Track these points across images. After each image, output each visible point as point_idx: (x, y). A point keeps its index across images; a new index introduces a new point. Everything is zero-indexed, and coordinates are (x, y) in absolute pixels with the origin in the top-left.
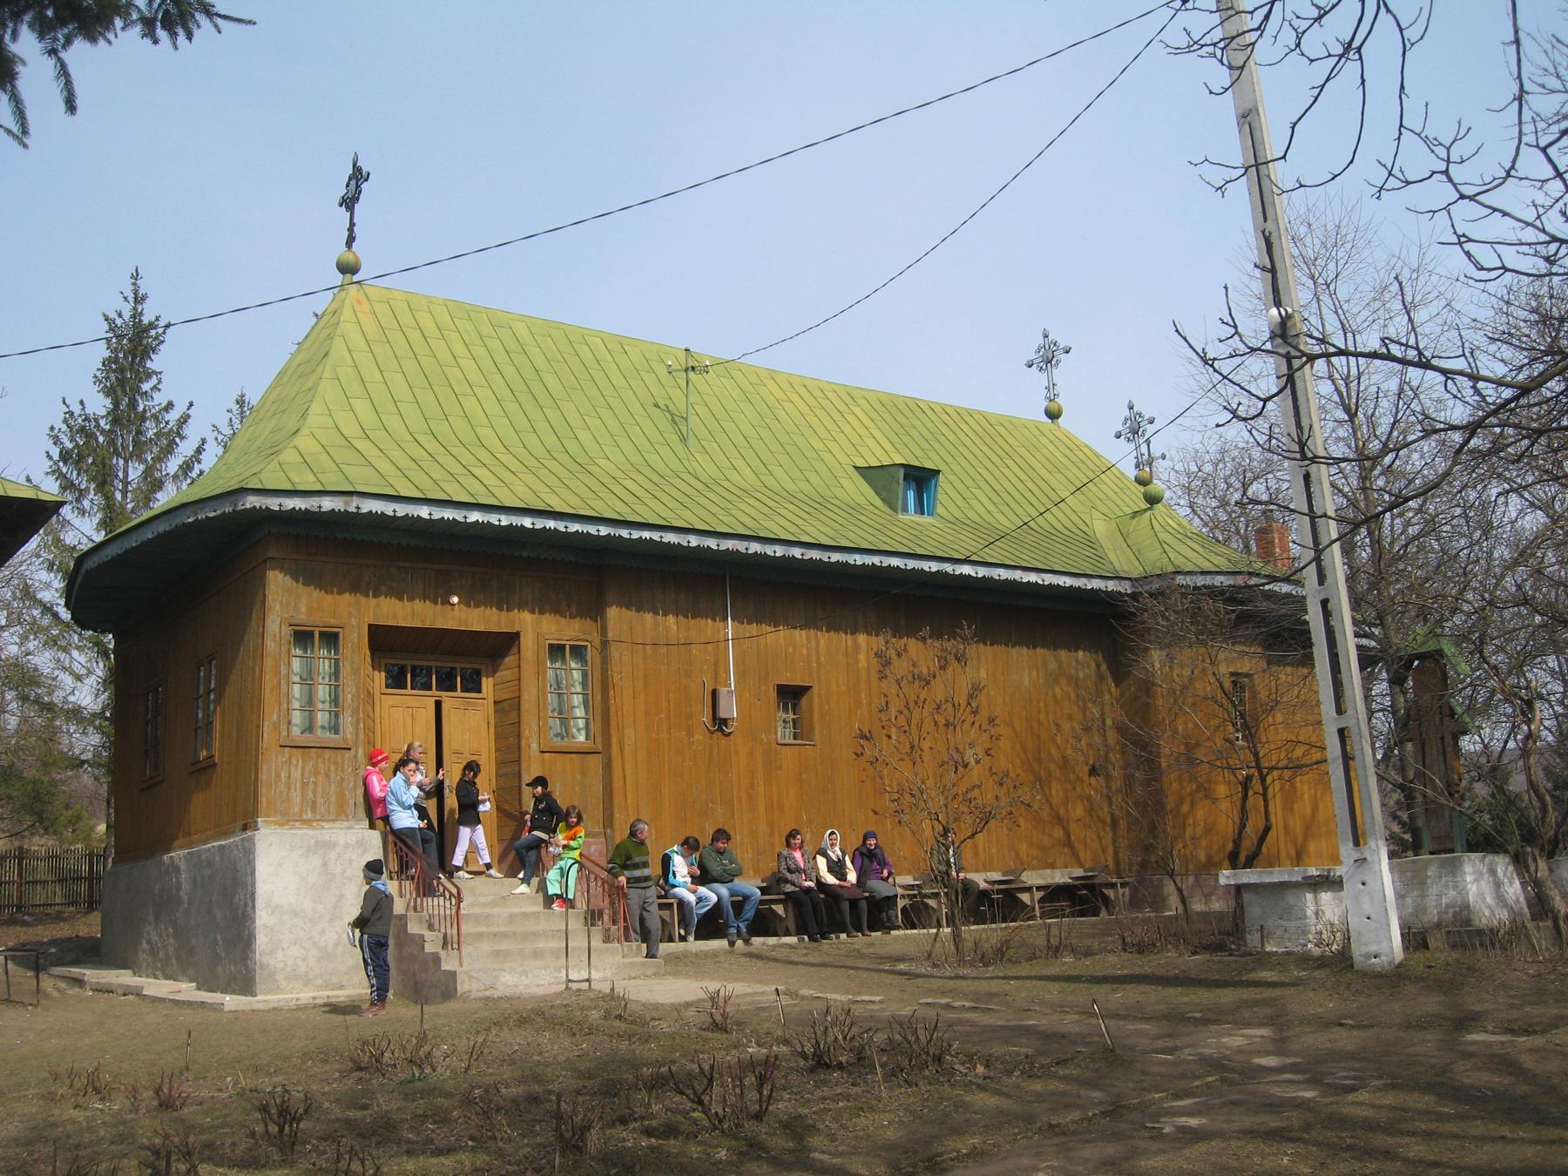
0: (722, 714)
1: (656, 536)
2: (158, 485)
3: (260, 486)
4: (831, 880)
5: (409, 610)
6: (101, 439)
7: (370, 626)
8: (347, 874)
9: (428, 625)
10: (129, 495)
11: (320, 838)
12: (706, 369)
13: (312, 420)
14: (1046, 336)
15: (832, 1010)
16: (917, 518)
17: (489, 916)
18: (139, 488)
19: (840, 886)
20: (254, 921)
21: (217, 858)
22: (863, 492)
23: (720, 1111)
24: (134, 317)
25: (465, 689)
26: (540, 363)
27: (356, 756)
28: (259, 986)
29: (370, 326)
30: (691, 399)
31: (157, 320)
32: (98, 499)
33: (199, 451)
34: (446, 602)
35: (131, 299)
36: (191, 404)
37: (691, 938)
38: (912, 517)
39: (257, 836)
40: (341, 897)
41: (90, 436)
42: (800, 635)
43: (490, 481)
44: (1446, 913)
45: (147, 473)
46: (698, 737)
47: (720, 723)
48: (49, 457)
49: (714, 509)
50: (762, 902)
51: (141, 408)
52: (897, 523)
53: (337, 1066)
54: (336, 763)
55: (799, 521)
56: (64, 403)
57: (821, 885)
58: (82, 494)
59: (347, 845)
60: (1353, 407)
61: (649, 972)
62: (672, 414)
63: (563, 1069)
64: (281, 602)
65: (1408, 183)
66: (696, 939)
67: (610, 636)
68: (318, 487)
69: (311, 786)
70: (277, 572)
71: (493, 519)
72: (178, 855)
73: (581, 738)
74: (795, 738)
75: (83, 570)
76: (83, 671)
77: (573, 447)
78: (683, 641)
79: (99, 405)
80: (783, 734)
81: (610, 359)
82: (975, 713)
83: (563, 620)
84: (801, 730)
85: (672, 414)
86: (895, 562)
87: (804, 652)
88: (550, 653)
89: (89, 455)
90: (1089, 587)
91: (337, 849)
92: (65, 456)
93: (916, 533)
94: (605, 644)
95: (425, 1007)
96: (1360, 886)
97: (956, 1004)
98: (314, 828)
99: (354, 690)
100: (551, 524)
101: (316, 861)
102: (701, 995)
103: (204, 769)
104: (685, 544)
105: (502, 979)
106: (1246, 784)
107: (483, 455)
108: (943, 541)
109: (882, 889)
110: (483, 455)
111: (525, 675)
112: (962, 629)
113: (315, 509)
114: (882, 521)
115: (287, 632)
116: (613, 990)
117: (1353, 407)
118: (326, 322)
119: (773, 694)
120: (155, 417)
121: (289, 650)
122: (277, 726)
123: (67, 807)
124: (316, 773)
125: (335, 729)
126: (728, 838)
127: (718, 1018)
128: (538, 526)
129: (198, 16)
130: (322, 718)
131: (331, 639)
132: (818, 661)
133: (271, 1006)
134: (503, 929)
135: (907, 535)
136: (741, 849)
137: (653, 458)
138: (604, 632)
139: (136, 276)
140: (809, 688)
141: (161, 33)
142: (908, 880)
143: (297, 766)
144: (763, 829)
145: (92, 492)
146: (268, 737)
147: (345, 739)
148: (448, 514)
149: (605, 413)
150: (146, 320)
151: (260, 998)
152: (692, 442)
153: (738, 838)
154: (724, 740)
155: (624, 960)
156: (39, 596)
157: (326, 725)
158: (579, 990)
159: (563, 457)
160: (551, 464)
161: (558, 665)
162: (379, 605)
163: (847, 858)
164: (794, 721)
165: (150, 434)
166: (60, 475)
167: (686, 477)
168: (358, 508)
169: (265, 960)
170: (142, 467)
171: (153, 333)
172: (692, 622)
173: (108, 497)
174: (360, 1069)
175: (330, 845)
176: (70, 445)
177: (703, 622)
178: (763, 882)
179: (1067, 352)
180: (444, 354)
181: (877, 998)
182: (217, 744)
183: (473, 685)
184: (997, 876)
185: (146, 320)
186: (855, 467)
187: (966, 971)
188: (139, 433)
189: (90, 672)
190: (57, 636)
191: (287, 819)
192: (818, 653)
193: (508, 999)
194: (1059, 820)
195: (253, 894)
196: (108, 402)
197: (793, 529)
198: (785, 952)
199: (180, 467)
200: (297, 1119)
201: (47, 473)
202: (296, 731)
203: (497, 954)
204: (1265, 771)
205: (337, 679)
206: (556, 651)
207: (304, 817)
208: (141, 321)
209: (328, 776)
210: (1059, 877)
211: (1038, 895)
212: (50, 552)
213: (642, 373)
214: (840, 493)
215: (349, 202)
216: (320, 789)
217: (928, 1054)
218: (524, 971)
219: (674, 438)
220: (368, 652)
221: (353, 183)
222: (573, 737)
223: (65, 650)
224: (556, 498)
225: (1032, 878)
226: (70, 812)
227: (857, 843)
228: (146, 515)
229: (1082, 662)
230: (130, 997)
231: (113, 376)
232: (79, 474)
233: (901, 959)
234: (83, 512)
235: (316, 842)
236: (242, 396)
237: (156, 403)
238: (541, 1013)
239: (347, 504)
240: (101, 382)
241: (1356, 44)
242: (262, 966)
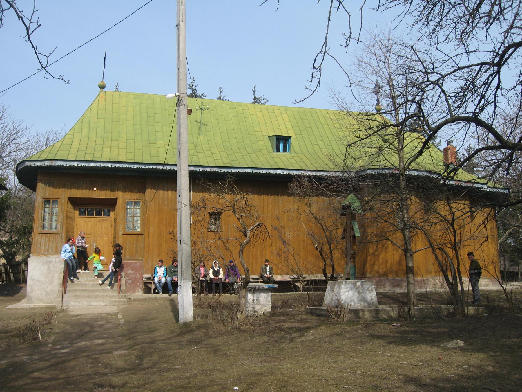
1: (154, 167)
5: (81, 193)
8: (55, 271)
9: (87, 197)
17: (86, 284)
27: (62, 236)
34: (93, 190)
37: (161, 293)
40: (53, 277)
61: (122, 304)
66: (162, 294)
69: (47, 245)
70: (40, 183)
71: (98, 165)
73: (139, 230)
83: (132, 194)
86: (248, 171)
91: (53, 263)
98: (47, 257)
100: (118, 165)
101: (46, 266)
105: (71, 304)
113: (43, 165)
148: (83, 164)
155: (119, 300)
168: (55, 164)
175: (50, 262)
191: (39, 254)
203: (76, 296)
207: (45, 254)
209: (53, 242)
218: (79, 301)
222: (136, 229)
239: (52, 163)
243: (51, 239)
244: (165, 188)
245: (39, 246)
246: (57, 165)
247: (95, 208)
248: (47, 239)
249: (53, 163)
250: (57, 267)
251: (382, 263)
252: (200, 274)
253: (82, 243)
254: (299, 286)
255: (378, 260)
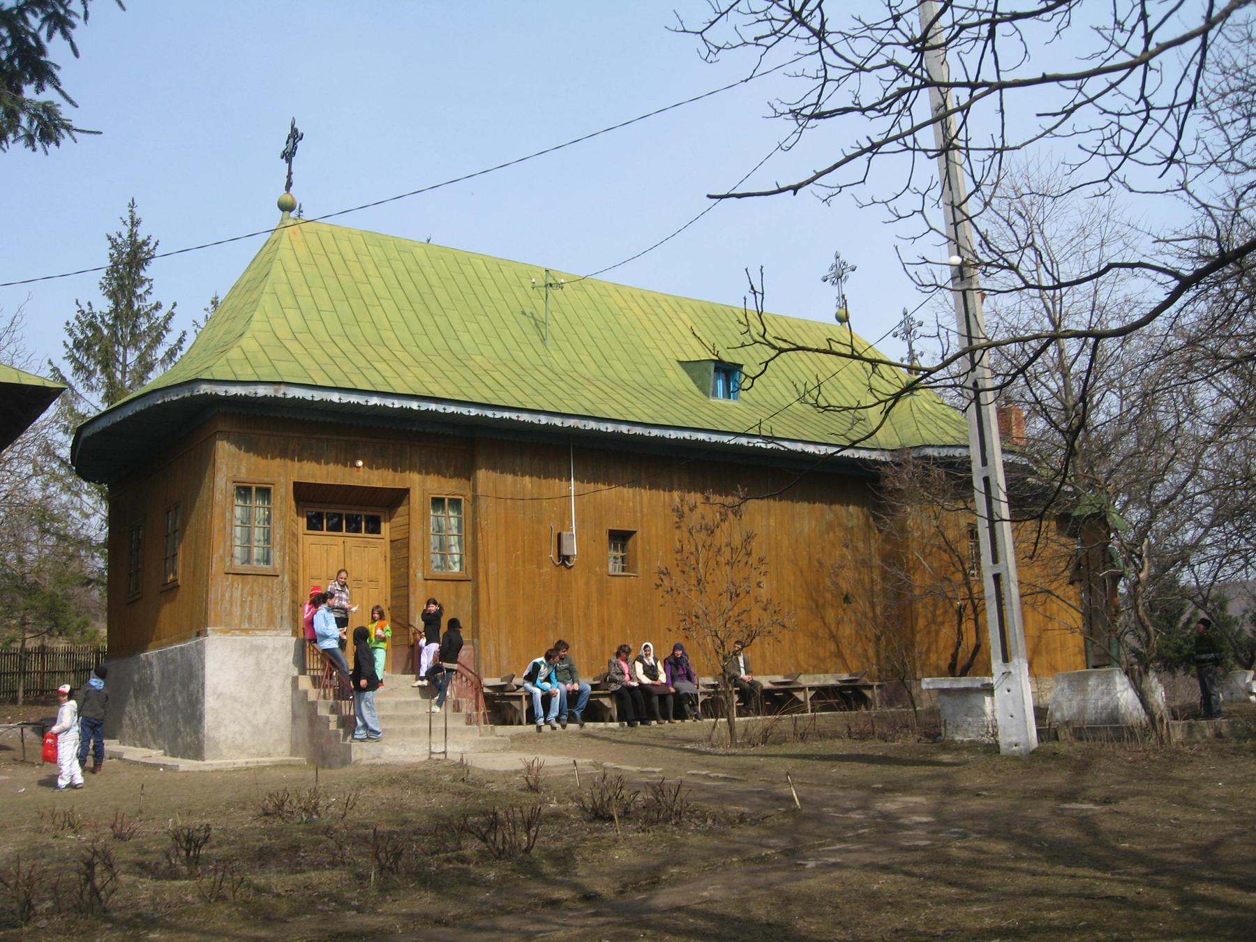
0: (565, 552)
1: (514, 416)
2: (150, 367)
3: (211, 378)
4: (646, 680)
6: (106, 332)
7: (295, 483)
10: (127, 375)
11: (254, 643)
12: (561, 286)
13: (255, 325)
14: (837, 258)
15: (608, 776)
16: (322, 510)
18: (134, 370)
19: (653, 685)
20: (203, 705)
21: (179, 657)
22: (683, 381)
23: (501, 847)
24: (130, 236)
25: (368, 531)
26: (434, 280)
27: (282, 582)
28: (207, 753)
29: (302, 252)
30: (550, 306)
31: (149, 238)
32: (104, 378)
33: (181, 341)
34: (354, 465)
35: (129, 223)
36: (175, 305)
38: (720, 401)
39: (206, 642)
40: (270, 687)
41: (96, 329)
42: (628, 492)
43: (388, 373)
44: (1101, 713)
45: (141, 358)
46: (546, 569)
47: (564, 559)
48: (66, 345)
49: (561, 394)
50: (592, 696)
51: (136, 308)
52: (708, 406)
53: (251, 812)
54: (267, 586)
55: (628, 404)
56: (77, 303)
57: (641, 684)
58: (90, 374)
59: (275, 649)
60: (1057, 321)
61: (499, 748)
62: (535, 320)
63: (658, 845)
64: (227, 465)
65: (900, 218)
67: (479, 491)
68: (255, 378)
69: (248, 604)
70: (225, 442)
71: (389, 402)
72: (151, 654)
73: (456, 569)
74: (623, 571)
75: (82, 438)
76: (91, 511)
77: (455, 346)
78: (535, 496)
79: (103, 305)
80: (613, 567)
81: (489, 276)
82: (749, 554)
84: (627, 564)
85: (535, 320)
86: (702, 436)
87: (631, 504)
88: (433, 503)
89: (96, 344)
90: (856, 456)
92: (78, 345)
93: (720, 413)
94: (475, 498)
95: (319, 769)
96: (1006, 692)
97: (712, 775)
99: (282, 532)
100: (433, 407)
101: (251, 660)
102: (521, 766)
103: (171, 589)
104: (537, 422)
105: (387, 751)
106: (960, 612)
107: (384, 352)
108: (742, 420)
109: (685, 687)
110: (384, 352)
111: (413, 521)
112: (737, 491)
114: (694, 404)
115: (231, 487)
116: (462, 759)
117: (1057, 321)
118: (268, 254)
119: (606, 537)
120: (147, 314)
121: (233, 501)
122: (222, 558)
123: (78, 615)
124: (252, 594)
125: (267, 561)
126: (567, 647)
127: (532, 782)
128: (423, 408)
129: (63, 131)
130: (257, 552)
131: (265, 493)
132: (641, 512)
133: (214, 768)
134: (390, 713)
135: (713, 415)
136: (577, 655)
137: (518, 355)
138: (475, 489)
139: (132, 205)
140: (635, 532)
141: (38, 144)
142: (710, 680)
143: (237, 588)
144: (596, 640)
145: (98, 372)
146: (216, 566)
147: (274, 569)
148: (354, 399)
149: (482, 319)
150: (140, 239)
151: (207, 762)
152: (549, 341)
153: (576, 647)
154: (566, 572)
155: (481, 738)
156: (57, 453)
157: (260, 558)
158: (438, 760)
159: (447, 355)
160: (436, 359)
161: (439, 513)
162: (301, 467)
163: (659, 664)
164: (623, 558)
165: (144, 327)
166: (75, 360)
167: (543, 369)
168: (285, 394)
169: (211, 734)
170: (137, 353)
171: (145, 249)
172: (543, 481)
173: (111, 377)
174: (267, 814)
176: (81, 337)
177: (551, 481)
178: (594, 680)
179: (854, 270)
180: (358, 274)
181: (657, 770)
182: (180, 571)
183: (374, 527)
184: (780, 679)
185: (140, 239)
186: (679, 362)
187: (734, 750)
188: (135, 326)
189: (96, 511)
190: (71, 483)
191: (229, 629)
192: (642, 507)
193: (388, 765)
194: (833, 637)
195: (203, 684)
196: (111, 303)
197: (623, 411)
198: (606, 734)
199: (167, 353)
200: (198, 847)
201: (64, 358)
202: (237, 562)
204: (976, 601)
205: (269, 523)
206: (438, 503)
207: (243, 627)
208: (135, 240)
209: (261, 596)
210: (830, 680)
211: (810, 694)
212: (66, 419)
213: (514, 288)
214: (664, 381)
215: (288, 156)
216: (255, 606)
217: (672, 810)
219: (535, 339)
220: (293, 503)
221: (291, 140)
222: (450, 568)
223: (77, 494)
224: (438, 387)
225: (805, 680)
226: (79, 619)
227: (669, 653)
228: (139, 391)
229: (852, 514)
230: (114, 760)
231: (114, 283)
232: (88, 359)
233: (689, 741)
234: (92, 388)
235: (251, 646)
236: (216, 298)
237: (148, 303)
238: (406, 776)
239: (276, 391)
240: (105, 287)
241: (908, 105)
242: (209, 739)
243: (256, 588)
244: (517, 468)
245: (229, 607)
246: (289, 396)
247: (344, 512)
248: (247, 588)
249: (280, 392)
250: (277, 661)
251: (945, 647)
252: (623, 673)
253: (340, 599)
254: (518, 708)
255: (937, 642)
